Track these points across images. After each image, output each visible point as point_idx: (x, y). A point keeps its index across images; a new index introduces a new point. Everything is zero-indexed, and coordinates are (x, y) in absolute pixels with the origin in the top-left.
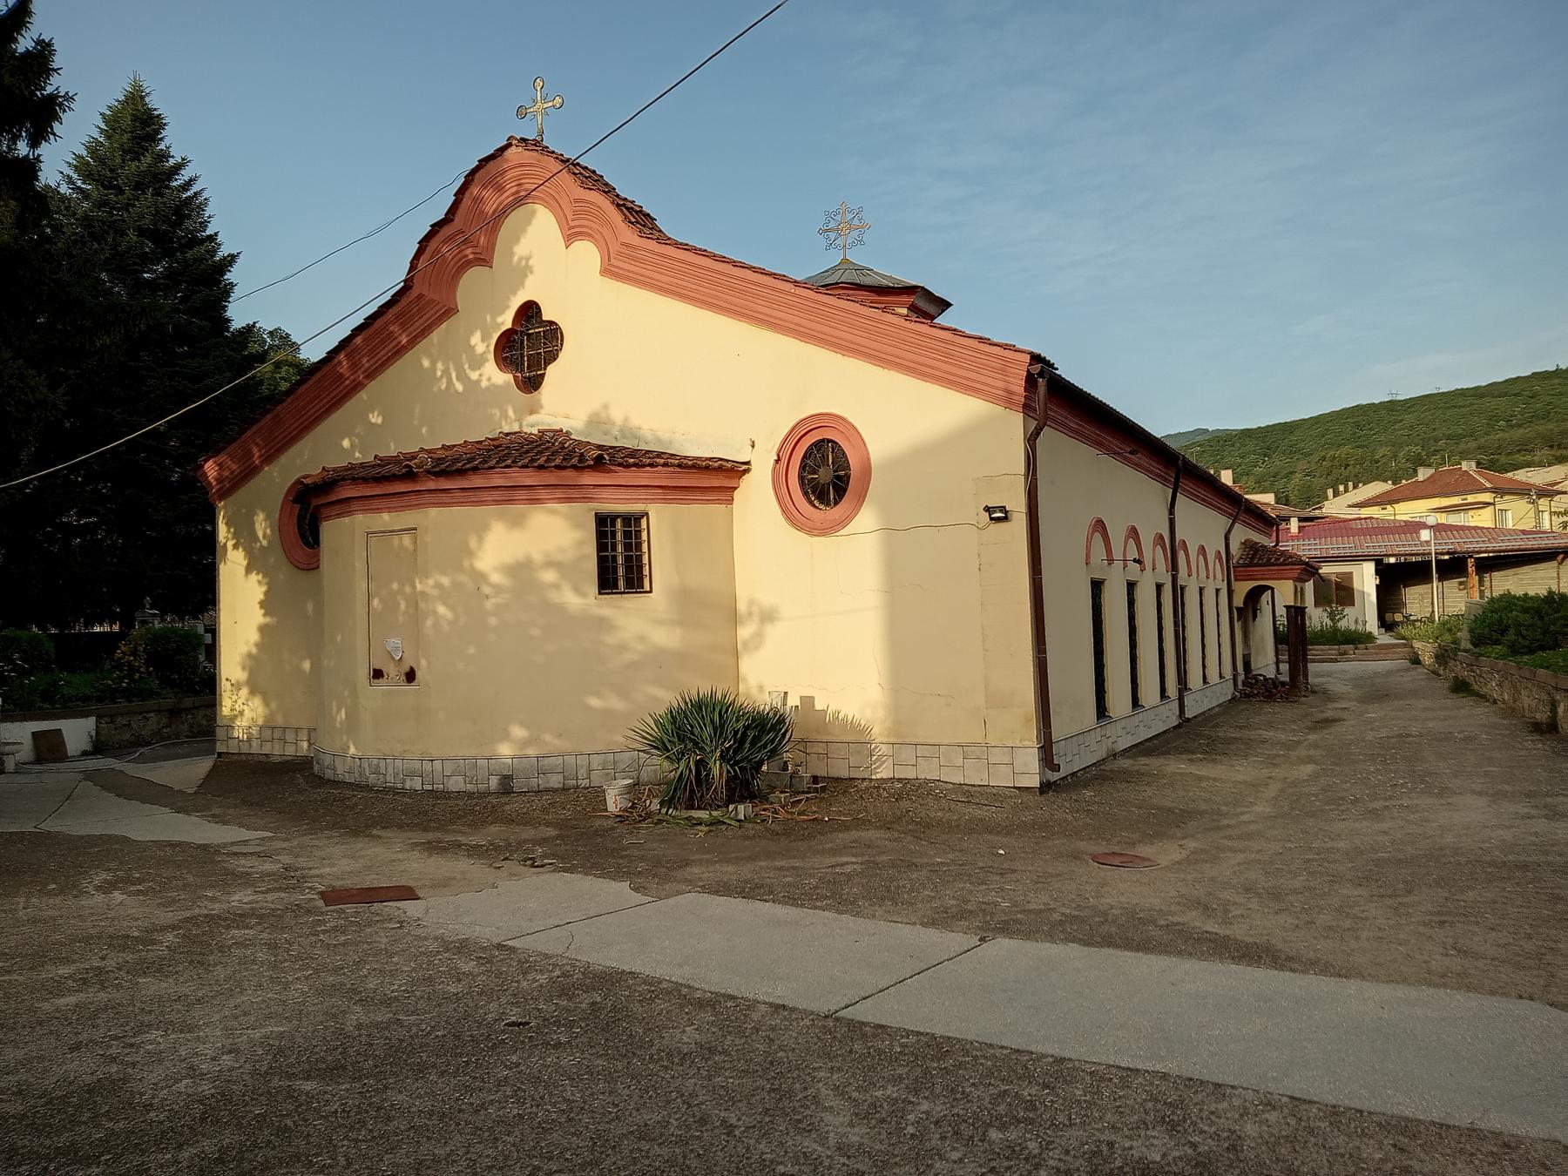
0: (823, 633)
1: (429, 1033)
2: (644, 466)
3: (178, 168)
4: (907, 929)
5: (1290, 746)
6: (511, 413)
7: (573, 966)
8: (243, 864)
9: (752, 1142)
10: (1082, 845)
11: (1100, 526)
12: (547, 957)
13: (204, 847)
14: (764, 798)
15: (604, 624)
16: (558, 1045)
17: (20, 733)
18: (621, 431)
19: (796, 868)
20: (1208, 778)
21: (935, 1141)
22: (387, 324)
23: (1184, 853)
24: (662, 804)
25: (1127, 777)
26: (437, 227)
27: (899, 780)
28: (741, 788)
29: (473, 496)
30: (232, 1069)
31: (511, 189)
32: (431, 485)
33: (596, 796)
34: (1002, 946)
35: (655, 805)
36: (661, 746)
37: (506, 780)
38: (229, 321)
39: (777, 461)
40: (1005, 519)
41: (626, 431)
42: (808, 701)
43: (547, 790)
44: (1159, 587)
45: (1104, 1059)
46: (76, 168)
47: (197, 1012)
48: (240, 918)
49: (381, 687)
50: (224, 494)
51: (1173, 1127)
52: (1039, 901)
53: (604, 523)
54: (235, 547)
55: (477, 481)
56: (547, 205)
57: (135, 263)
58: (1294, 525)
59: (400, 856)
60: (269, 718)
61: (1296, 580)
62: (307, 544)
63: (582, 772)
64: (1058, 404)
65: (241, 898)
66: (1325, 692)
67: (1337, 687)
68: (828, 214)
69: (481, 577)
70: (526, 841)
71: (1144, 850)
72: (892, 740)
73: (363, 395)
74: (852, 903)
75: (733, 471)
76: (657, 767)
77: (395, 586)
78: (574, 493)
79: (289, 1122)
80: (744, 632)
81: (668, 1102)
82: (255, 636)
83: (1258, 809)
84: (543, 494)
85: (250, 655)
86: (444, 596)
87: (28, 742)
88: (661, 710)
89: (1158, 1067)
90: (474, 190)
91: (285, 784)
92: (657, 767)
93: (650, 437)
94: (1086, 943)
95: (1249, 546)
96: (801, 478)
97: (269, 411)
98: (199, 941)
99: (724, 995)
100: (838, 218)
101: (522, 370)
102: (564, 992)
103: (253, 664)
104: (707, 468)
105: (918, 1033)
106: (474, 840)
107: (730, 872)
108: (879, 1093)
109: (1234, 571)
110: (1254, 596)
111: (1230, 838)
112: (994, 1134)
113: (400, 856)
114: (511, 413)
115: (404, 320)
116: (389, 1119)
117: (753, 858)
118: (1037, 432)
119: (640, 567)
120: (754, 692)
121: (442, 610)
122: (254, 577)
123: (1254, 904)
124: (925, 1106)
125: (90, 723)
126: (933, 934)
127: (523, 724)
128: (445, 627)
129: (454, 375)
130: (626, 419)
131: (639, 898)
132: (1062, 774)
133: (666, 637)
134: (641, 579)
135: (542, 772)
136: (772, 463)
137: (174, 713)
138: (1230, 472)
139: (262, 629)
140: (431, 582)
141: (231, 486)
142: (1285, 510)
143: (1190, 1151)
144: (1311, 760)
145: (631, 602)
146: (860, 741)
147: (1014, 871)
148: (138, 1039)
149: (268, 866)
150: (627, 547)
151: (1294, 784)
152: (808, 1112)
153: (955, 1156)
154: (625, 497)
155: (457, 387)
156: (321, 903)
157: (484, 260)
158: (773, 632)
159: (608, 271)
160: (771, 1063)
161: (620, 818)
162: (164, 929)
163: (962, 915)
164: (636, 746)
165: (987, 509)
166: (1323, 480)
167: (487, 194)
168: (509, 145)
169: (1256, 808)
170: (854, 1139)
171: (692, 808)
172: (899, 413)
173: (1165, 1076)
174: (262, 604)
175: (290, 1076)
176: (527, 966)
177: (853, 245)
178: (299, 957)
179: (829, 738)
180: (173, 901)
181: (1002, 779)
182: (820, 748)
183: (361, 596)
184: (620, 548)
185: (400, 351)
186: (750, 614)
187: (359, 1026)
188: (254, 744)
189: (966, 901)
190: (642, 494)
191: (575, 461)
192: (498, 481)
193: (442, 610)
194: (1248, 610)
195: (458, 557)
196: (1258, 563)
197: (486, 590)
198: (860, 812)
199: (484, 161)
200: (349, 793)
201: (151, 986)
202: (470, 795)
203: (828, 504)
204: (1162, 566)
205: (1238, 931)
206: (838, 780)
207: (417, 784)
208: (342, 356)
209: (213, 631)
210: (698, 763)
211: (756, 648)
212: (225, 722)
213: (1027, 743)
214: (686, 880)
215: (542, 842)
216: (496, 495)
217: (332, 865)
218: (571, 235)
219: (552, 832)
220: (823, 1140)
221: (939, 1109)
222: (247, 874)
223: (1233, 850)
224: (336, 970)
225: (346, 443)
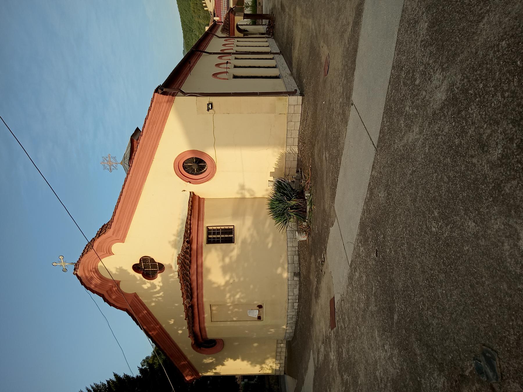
0: (248, 169)
1: (379, 282)
2: (190, 227)
4: (348, 131)
5: (290, 16)
6: (172, 275)
7: (358, 240)
8: (321, 357)
9: (418, 163)
10: (321, 80)
11: (215, 75)
12: (355, 249)
13: (315, 372)
14: (303, 188)
15: (244, 242)
16: (384, 238)
18: (178, 237)
19: (327, 173)
20: (300, 42)
21: (419, 102)
23: (325, 45)
24: (305, 221)
25: (298, 70)
26: (105, 300)
27: (299, 143)
28: (300, 195)
29: (200, 286)
30: (390, 345)
32: (195, 300)
33: (301, 244)
34: (355, 98)
35: (305, 224)
36: (286, 222)
37: (295, 274)
38: (137, 376)
39: (190, 182)
40: (212, 104)
41: (178, 235)
42: (272, 174)
43: (299, 261)
44: (236, 59)
45: (393, 53)
47: (370, 361)
48: (339, 354)
49: (264, 317)
50: (197, 373)
51: (416, 22)
52: (340, 89)
53: (210, 241)
54: (215, 369)
55: (194, 284)
58: (216, 19)
59: (320, 306)
60: (272, 357)
62: (215, 345)
63: (294, 249)
64: (173, 85)
65: (333, 356)
66: (272, 9)
67: (270, 6)
69: (227, 283)
70: (316, 265)
71: (323, 59)
73: (164, 326)
74: (339, 151)
75: (193, 197)
76: (292, 224)
77: (230, 312)
78: (199, 251)
79: (408, 320)
80: (248, 196)
81: (404, 195)
82: (245, 362)
83: (310, 23)
84: (199, 262)
85: (251, 364)
88: (274, 221)
89: (396, 33)
90: (92, 287)
91: (295, 349)
92: (292, 224)
93: (180, 227)
94: (354, 69)
95: (223, 31)
96: (196, 174)
98: (347, 366)
99: (369, 187)
100: (106, 165)
101: (157, 271)
102: (366, 240)
103: (254, 363)
104: (192, 206)
105: (383, 118)
106: (315, 283)
107: (327, 195)
108: (403, 125)
109: (231, 36)
110: (240, 30)
111: (320, 31)
112: (417, 82)
113: (320, 306)
114: (172, 275)
115: (138, 312)
116: (408, 286)
117: (323, 188)
118: (182, 92)
119: (225, 229)
120: (268, 192)
121: (238, 296)
122: (226, 363)
123: (342, 17)
124: (407, 108)
126: (350, 122)
127: (277, 269)
128: (242, 295)
129: (158, 295)
130: (174, 235)
131: (336, 223)
132: (298, 89)
133: (249, 221)
134: (229, 229)
135: (293, 263)
136: (191, 184)
139: (243, 360)
140: (228, 301)
141: (194, 371)
142: (211, 21)
143: (425, 14)
144: (295, 9)
145: (237, 233)
146: (285, 157)
147: (329, 100)
148: (379, 379)
149: (322, 350)
150: (218, 233)
151: (302, 13)
152: (408, 147)
153: (424, 93)
154: (201, 235)
155: (162, 292)
156: (335, 329)
157: (117, 283)
158: (247, 186)
159: (123, 241)
160: (391, 164)
161: (309, 235)
162: (342, 379)
163: (344, 114)
164: (285, 230)
165: (208, 110)
166: (201, 12)
167: (94, 282)
169: (310, 25)
170: (417, 129)
171: (306, 212)
172: (173, 141)
173: (399, 30)
174: (235, 360)
175: (392, 324)
176: (357, 255)
177: (115, 160)
178: (353, 332)
179: (284, 167)
180: (334, 379)
181: (299, 109)
182: (288, 170)
183: (232, 324)
184: (219, 236)
185: (149, 313)
186: (242, 193)
187: (376, 306)
188: (281, 362)
189: (339, 114)
191: (188, 251)
193: (238, 296)
194: (245, 33)
196: (229, 28)
197: (231, 281)
198: (309, 156)
200: (299, 327)
201: (362, 379)
202: (300, 286)
203: (205, 165)
204: (229, 57)
205: (351, 20)
206: (298, 164)
207: (296, 305)
209: (244, 377)
210: (291, 209)
211: (253, 191)
212: (274, 372)
213: (287, 100)
214: (330, 209)
215: (316, 260)
217: (322, 328)
219: (313, 258)
220: (417, 140)
221: (409, 103)
222: (324, 356)
223: (324, 29)
224: (357, 318)
225: (180, 332)
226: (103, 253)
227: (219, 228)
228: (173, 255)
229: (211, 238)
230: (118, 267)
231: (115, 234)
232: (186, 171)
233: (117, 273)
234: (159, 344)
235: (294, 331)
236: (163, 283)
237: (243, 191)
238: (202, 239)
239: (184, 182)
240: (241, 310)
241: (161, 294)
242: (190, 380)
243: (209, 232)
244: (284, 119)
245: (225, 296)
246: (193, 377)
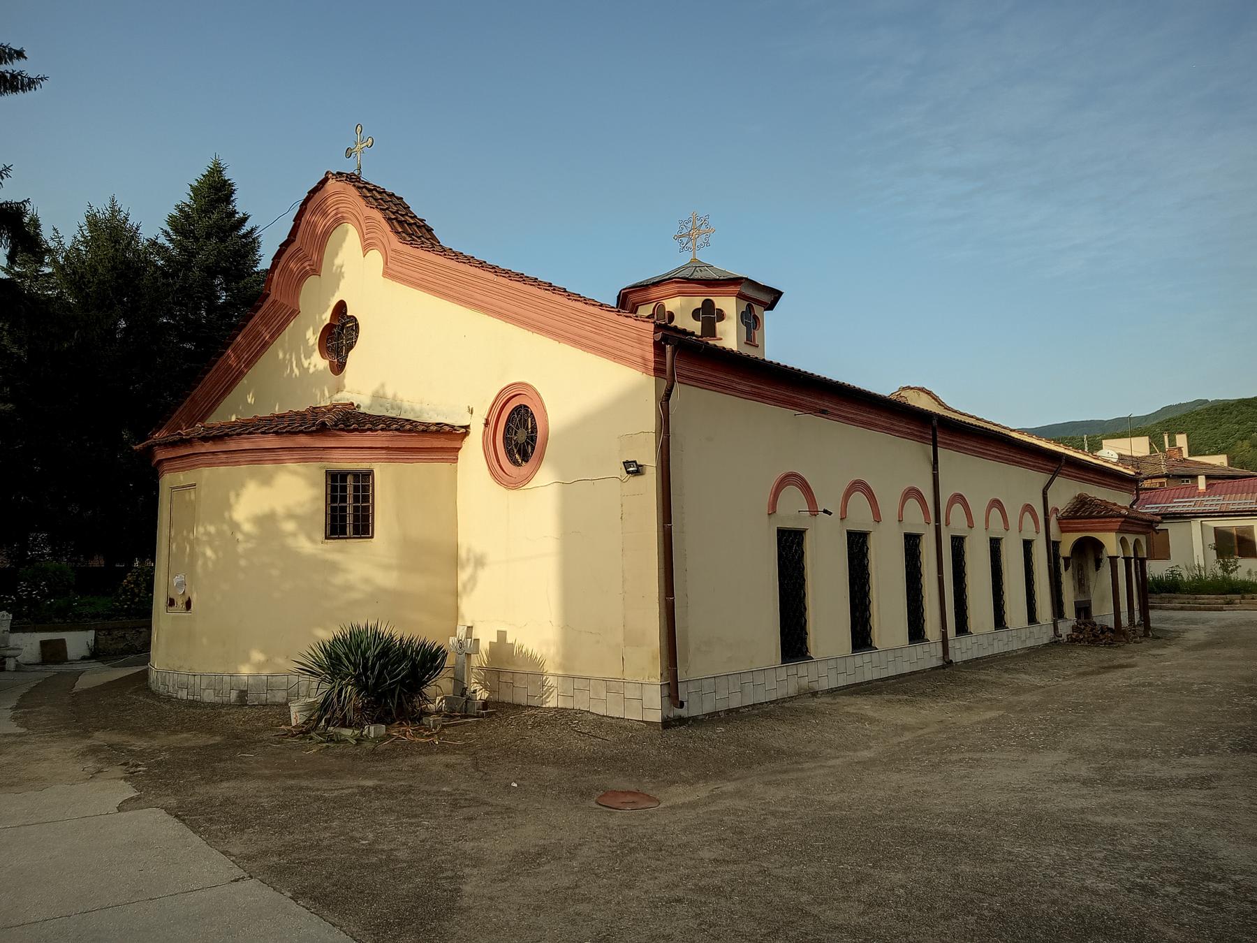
3: (244, 220)
15: (334, 567)
17: (29, 644)
22: (255, 325)
29: (233, 457)
37: (243, 694)
44: (1027, 544)
53: (336, 481)
55: (232, 445)
61: (1119, 531)
68: (681, 222)
69: (235, 526)
72: (560, 673)
73: (245, 381)
75: (457, 434)
80: (463, 576)
84: (284, 455)
87: (36, 648)
90: (307, 216)
97: (188, 395)
121: (209, 553)
125: (91, 635)
127: (262, 651)
128: (210, 564)
130: (395, 396)
133: (387, 579)
135: (270, 687)
138: (1184, 437)
140: (201, 530)
150: (356, 499)
157: (316, 271)
158: (483, 575)
159: (386, 274)
181: (634, 715)
185: (265, 346)
186: (468, 560)
192: (246, 446)
193: (209, 553)
197: (240, 536)
199: (313, 192)
207: (183, 694)
211: (472, 590)
213: (653, 680)
216: (249, 456)
232: (512, 413)
237: (472, 564)
241: (296, 371)
244: (613, 671)
245: (211, 523)
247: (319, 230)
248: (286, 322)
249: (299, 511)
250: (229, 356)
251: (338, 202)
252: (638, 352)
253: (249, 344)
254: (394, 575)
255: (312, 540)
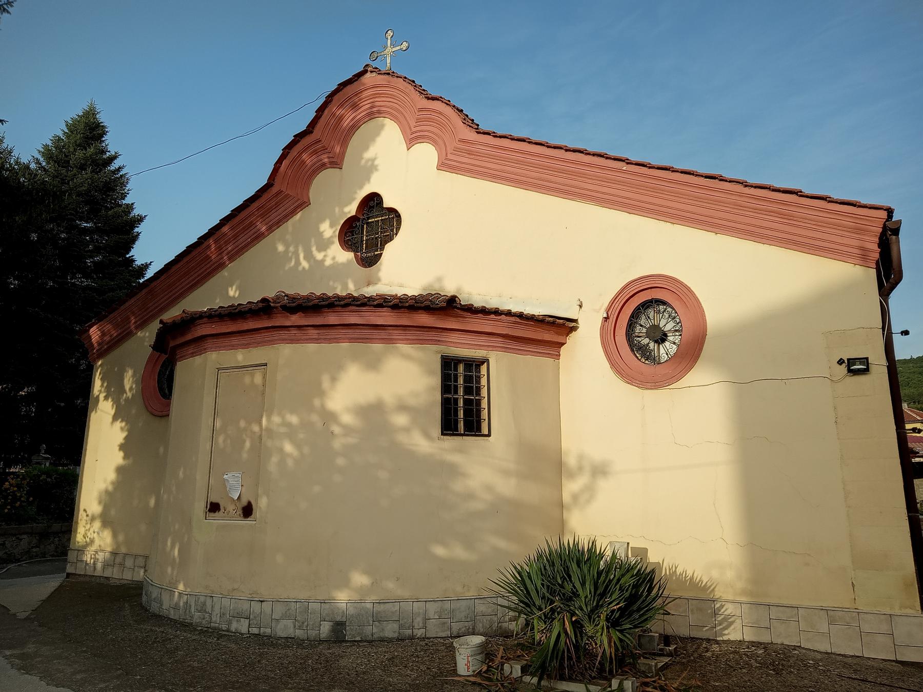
3: (115, 157)
15: (453, 471)
24: (524, 670)
31: (365, 106)
37: (339, 626)
40: (866, 371)
43: (382, 640)
46: (43, 154)
49: (216, 520)
50: (101, 354)
53: (449, 364)
54: (106, 398)
56: (395, 118)
57: (71, 214)
63: (419, 621)
69: (330, 417)
73: (225, 273)
80: (570, 488)
82: (112, 476)
84: (396, 334)
85: (107, 491)
86: (291, 433)
90: (333, 108)
103: (109, 499)
115: (264, 214)
119: (479, 412)
121: (288, 448)
127: (366, 572)
128: (290, 462)
129: (302, 256)
133: (507, 487)
135: (377, 618)
137: (44, 536)
139: (120, 470)
140: (276, 419)
141: (108, 347)
146: (704, 600)
150: (468, 390)
155: (313, 254)
157: (336, 163)
158: (603, 485)
159: (444, 165)
168: (364, 72)
184: (461, 391)
185: (259, 237)
190: (482, 340)
193: (288, 448)
195: (310, 394)
197: (336, 429)
207: (242, 626)
208: (211, 241)
213: (909, 611)
218: (412, 139)
226: (413, 123)
227: (484, 392)
228: (401, 286)
229: (456, 369)
230: (376, 162)
231: (461, 146)
233: (363, 162)
234: (181, 263)
235: (164, 613)
236: (332, 267)
238: (456, 344)
239: (606, 304)
240: (245, 455)
241: (305, 264)
242: (90, 337)
243: (474, 365)
246: (96, 345)
247: (346, 122)
248: (293, 213)
249: (412, 402)
250: (209, 247)
251: (375, 96)
252: (856, 243)
253: (236, 236)
254: (513, 481)
255: (427, 435)
